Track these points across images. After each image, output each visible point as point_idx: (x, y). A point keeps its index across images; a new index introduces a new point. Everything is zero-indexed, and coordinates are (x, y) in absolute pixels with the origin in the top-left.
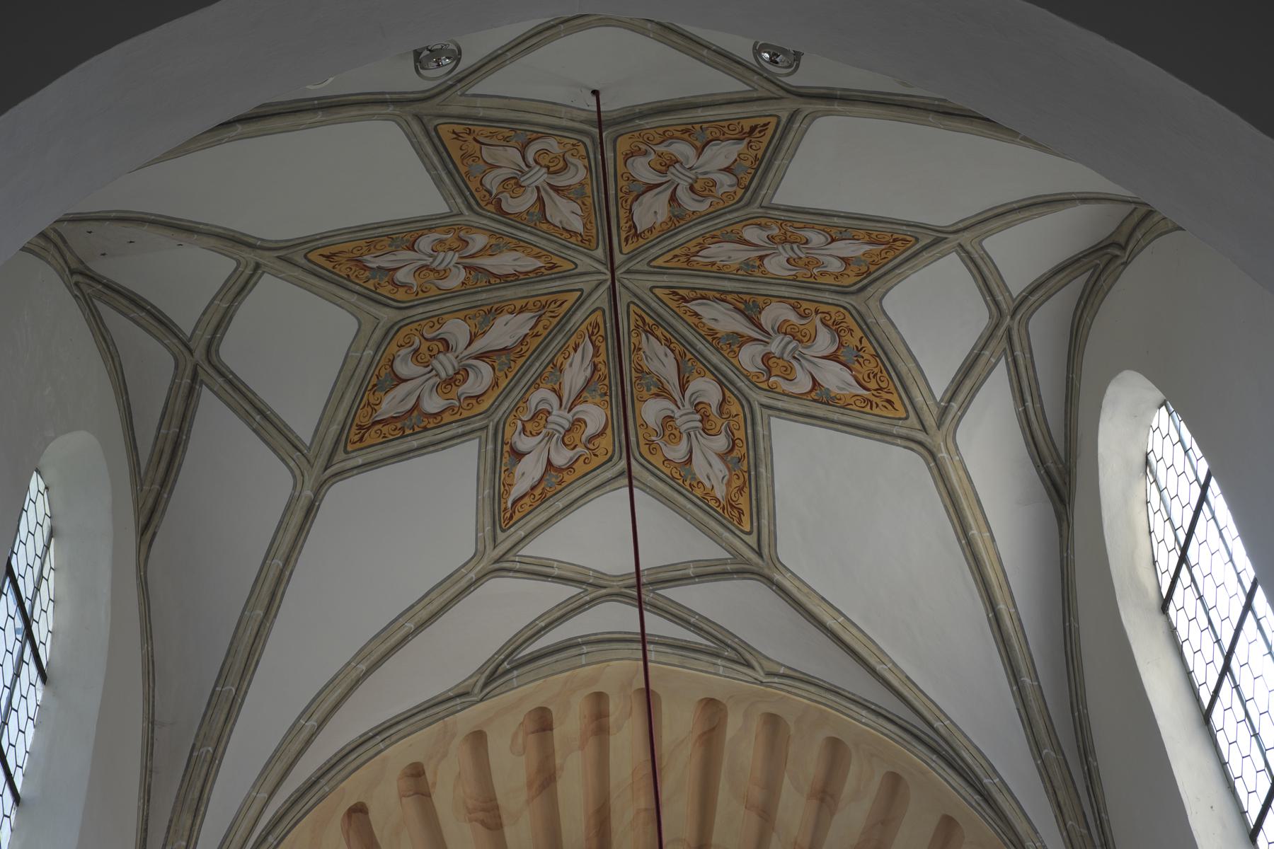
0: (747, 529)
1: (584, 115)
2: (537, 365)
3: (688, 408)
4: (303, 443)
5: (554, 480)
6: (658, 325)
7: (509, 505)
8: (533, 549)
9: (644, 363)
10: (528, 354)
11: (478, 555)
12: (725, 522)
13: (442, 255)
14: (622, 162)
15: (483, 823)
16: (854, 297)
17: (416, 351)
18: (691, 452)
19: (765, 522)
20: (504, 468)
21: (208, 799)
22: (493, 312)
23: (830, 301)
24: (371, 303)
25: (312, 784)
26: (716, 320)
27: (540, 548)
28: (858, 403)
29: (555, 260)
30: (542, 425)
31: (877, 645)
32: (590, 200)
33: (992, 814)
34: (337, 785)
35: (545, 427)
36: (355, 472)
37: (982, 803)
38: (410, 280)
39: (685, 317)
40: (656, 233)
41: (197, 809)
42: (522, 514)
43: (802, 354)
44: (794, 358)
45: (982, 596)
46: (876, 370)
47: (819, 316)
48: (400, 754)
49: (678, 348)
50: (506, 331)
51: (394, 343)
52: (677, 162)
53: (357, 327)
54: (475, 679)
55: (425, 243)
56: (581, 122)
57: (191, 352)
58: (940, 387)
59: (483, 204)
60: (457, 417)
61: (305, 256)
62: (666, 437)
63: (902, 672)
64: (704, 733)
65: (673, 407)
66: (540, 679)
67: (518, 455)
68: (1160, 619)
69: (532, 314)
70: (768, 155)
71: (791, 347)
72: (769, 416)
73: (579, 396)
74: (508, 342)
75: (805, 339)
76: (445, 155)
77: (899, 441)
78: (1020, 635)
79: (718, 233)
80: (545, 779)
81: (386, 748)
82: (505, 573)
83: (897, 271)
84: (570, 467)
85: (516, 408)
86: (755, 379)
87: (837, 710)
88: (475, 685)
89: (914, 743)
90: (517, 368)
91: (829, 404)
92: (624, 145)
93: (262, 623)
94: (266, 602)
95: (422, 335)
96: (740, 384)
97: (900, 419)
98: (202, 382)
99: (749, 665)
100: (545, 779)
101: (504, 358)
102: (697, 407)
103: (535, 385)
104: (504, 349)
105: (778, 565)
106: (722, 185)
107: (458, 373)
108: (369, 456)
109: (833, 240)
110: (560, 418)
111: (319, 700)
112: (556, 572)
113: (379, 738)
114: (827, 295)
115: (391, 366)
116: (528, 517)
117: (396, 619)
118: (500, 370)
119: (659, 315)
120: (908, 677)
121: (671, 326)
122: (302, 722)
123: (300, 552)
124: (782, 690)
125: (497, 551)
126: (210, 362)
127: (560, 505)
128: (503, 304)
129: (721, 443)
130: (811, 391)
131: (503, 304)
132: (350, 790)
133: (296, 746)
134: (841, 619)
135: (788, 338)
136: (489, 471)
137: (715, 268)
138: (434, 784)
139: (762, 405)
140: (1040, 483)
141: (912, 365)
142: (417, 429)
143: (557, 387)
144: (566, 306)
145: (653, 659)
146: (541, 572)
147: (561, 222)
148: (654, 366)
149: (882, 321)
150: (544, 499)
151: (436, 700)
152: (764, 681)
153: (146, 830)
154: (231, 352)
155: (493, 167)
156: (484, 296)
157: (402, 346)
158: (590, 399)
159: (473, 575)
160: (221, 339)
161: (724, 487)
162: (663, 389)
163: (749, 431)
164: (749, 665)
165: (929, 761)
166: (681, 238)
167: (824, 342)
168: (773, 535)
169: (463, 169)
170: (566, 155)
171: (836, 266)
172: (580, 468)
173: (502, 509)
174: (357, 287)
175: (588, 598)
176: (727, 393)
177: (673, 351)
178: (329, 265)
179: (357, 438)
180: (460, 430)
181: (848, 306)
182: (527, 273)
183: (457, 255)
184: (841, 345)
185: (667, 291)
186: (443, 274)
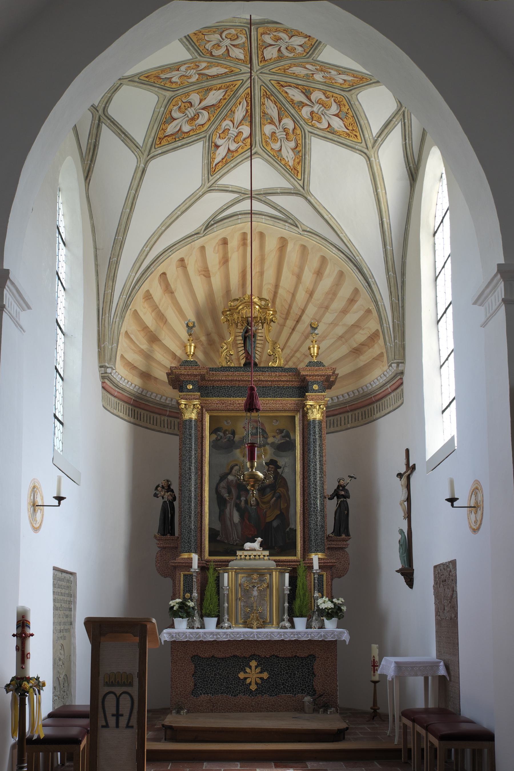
0: (300, 178)
1: (245, 20)
2: (225, 111)
3: (281, 129)
4: (140, 145)
5: (230, 155)
6: (272, 95)
7: (214, 166)
8: (221, 182)
9: (266, 110)
10: (221, 107)
11: (203, 185)
12: (292, 175)
13: (189, 71)
14: (260, 36)
15: (204, 275)
16: (347, 93)
17: (180, 107)
18: (281, 146)
19: (306, 176)
20: (212, 152)
21: (117, 276)
22: (208, 90)
23: (338, 93)
24: (163, 90)
25: (148, 268)
26: (294, 95)
27: (225, 181)
28: (344, 134)
29: (233, 69)
30: (226, 134)
31: (341, 227)
32: (247, 48)
33: (370, 291)
34: (156, 268)
35: (227, 135)
36: (159, 156)
37: (368, 287)
38: (177, 80)
39: (282, 93)
40: (272, 61)
41: (113, 280)
42: (219, 169)
43: (325, 113)
44: (322, 114)
45: (378, 215)
46: (352, 122)
47: (333, 98)
48: (176, 256)
49: (279, 105)
50: (213, 97)
51: (171, 105)
52: (281, 39)
53: (157, 99)
54: (201, 227)
55: (183, 68)
56: (244, 23)
57: (98, 111)
58: (375, 131)
59: (205, 54)
60: (195, 133)
61: (139, 78)
62: (273, 140)
63: (348, 238)
64: (280, 247)
65: (276, 128)
66: (224, 228)
67: (217, 147)
68: (432, 238)
69: (224, 90)
70: (316, 44)
71: (322, 109)
72: (311, 136)
73: (241, 122)
74: (214, 102)
75: (327, 107)
76: (191, 41)
77: (358, 151)
78: (389, 231)
79: (297, 64)
80: (225, 261)
81: (172, 254)
82: (212, 191)
83: (363, 87)
84: (236, 150)
85: (217, 128)
86: (307, 121)
87: (325, 247)
88: (201, 230)
89: (349, 262)
90: (218, 112)
91: (333, 133)
92: (260, 30)
93: (129, 214)
94: (130, 207)
95: (182, 101)
96: (301, 122)
97: (359, 143)
98: (102, 122)
99: (297, 227)
100: (225, 261)
101: (212, 109)
102: (285, 129)
103: (224, 119)
104: (213, 105)
105: (310, 193)
106: (298, 50)
107: (195, 116)
108: (163, 149)
109: (340, 74)
110: (233, 132)
111: (150, 240)
112: (230, 189)
113: (169, 250)
114: (337, 90)
115: (171, 114)
116: (221, 171)
117: (174, 211)
118: (211, 114)
119: (272, 92)
120: (350, 240)
121: (277, 96)
122: (144, 248)
123: (140, 187)
124: (308, 238)
125: (209, 183)
126: (105, 115)
127: (232, 165)
128: (213, 86)
129: (292, 144)
130: (327, 128)
131: (213, 86)
132: (161, 269)
133: (143, 257)
134: (330, 216)
135: (321, 106)
136: (206, 153)
137: (295, 75)
138: (188, 264)
139: (309, 132)
140: (407, 172)
141: (366, 122)
142: (180, 138)
143: (232, 119)
144: (237, 86)
145: (258, 339)
146: (225, 190)
147: (235, 56)
148: (269, 111)
149: (357, 103)
150: (226, 163)
151: (188, 236)
152: (302, 233)
153: (98, 285)
154: (112, 111)
155: (209, 41)
156: (205, 84)
157: (174, 105)
158: (245, 124)
159: (201, 193)
160: (108, 106)
161: (293, 162)
162: (272, 121)
163: (303, 141)
164: (297, 227)
165: (353, 270)
166: (282, 63)
167: (334, 109)
168: (309, 181)
169: (197, 44)
170: (238, 34)
171: (341, 81)
172: (240, 151)
173: (211, 167)
174: (158, 85)
175: (241, 198)
176: (296, 126)
177: (277, 106)
178: (147, 79)
179: (159, 143)
180: (196, 138)
181: (345, 96)
182: (222, 74)
183: (195, 70)
184: (340, 111)
185: (276, 82)
186: (190, 77)
